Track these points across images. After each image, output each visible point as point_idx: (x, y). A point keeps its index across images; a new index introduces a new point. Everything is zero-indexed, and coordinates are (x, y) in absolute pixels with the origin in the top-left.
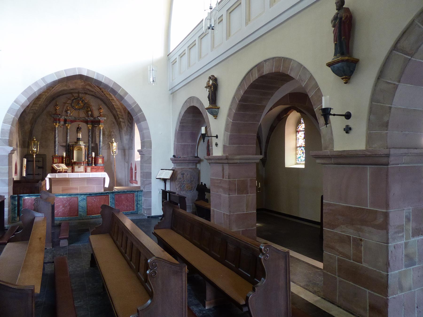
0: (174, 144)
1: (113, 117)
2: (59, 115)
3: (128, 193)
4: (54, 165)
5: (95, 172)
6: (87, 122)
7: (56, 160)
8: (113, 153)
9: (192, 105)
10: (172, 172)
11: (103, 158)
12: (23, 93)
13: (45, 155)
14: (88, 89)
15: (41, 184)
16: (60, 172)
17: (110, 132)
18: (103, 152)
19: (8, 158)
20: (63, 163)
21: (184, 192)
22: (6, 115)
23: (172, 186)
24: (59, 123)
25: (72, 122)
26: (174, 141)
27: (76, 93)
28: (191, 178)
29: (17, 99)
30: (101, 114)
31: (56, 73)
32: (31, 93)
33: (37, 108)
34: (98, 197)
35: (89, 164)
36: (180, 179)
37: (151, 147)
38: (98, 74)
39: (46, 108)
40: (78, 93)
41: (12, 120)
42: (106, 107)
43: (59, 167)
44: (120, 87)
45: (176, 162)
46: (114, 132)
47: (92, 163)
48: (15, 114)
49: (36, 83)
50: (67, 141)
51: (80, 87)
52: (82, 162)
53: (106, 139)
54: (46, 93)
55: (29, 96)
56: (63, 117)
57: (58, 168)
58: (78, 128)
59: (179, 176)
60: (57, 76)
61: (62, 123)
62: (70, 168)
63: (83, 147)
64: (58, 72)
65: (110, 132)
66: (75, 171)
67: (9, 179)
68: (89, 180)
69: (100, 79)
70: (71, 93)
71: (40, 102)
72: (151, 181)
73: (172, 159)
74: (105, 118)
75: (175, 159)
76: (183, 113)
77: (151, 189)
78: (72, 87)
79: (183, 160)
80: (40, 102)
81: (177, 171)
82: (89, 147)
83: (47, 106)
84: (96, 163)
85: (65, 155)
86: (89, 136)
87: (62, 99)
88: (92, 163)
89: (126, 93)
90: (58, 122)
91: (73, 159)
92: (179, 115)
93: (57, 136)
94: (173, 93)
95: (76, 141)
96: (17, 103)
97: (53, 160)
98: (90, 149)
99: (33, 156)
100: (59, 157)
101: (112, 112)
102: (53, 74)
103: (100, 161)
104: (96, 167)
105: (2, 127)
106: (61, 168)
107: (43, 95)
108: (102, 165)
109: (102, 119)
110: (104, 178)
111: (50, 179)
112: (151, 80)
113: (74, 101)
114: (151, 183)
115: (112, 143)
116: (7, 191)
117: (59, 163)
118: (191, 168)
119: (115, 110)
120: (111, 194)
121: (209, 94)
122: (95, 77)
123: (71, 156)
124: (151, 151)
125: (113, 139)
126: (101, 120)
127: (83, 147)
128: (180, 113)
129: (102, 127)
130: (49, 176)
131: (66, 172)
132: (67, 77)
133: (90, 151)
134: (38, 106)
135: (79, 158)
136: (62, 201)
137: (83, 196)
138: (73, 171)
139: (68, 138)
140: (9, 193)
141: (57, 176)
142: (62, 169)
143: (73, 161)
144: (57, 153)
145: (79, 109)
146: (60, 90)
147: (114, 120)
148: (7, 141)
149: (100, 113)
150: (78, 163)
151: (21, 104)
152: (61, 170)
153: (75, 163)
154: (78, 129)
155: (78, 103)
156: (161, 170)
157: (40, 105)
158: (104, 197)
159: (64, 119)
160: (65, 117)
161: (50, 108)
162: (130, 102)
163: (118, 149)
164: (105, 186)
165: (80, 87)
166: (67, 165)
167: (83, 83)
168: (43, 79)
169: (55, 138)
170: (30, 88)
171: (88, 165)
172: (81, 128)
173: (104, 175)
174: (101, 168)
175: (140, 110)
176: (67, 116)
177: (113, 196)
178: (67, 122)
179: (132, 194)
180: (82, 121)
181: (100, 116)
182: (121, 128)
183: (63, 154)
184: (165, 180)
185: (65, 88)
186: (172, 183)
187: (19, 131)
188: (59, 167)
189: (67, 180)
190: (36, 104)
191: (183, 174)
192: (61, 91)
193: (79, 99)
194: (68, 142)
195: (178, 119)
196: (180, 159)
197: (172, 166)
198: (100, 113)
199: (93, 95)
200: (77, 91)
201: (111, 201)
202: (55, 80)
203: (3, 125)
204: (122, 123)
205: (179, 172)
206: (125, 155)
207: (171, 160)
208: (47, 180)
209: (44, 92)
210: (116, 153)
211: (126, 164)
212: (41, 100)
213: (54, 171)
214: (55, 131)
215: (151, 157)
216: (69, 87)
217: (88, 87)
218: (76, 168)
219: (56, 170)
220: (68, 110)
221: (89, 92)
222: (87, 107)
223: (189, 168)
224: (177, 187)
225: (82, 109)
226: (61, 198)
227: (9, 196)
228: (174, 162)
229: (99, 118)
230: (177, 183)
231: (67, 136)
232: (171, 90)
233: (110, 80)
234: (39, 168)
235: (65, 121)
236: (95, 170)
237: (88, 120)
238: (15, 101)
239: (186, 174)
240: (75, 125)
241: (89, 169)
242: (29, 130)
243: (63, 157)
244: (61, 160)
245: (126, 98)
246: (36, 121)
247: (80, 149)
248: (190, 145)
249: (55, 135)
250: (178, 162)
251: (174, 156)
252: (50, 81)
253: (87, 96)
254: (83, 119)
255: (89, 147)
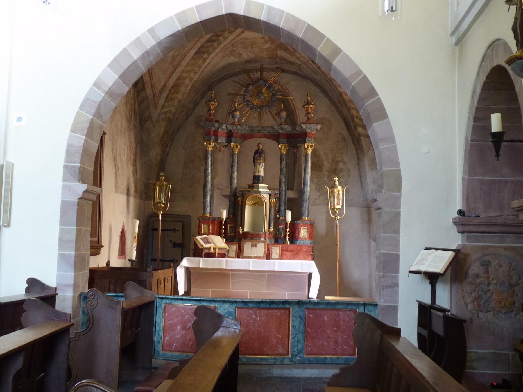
0: (463, 179)
1: (343, 124)
2: (217, 121)
3: (339, 307)
4: (198, 238)
5: (290, 259)
6: (276, 137)
7: (205, 228)
8: (334, 213)
9: (495, 64)
10: (449, 256)
11: (311, 226)
12: (110, 66)
13: (188, 217)
14: (284, 59)
15: (151, 276)
16: (210, 255)
17: (335, 162)
18: (312, 211)
19: (76, 207)
20: (220, 234)
21: (489, 315)
22: (78, 114)
23: (453, 298)
24: (216, 141)
25: (245, 137)
26: (464, 173)
27: (257, 70)
28: (511, 277)
29: (99, 78)
30: (310, 116)
31: (179, 16)
32: (126, 64)
33: (173, 109)
34: (263, 312)
35: (277, 239)
36: (477, 276)
37: (399, 188)
38: (270, 8)
39: (194, 109)
40: (261, 70)
41: (87, 125)
42: (325, 100)
43: (207, 242)
44: (321, 36)
45: (467, 228)
46: (344, 163)
47: (286, 236)
48: (93, 111)
49: (137, 42)
50: (231, 183)
51: (265, 54)
52: (262, 233)
53: (326, 179)
54: (192, 75)
55: (122, 71)
56: (224, 127)
57: (205, 246)
58: (257, 152)
59: (475, 269)
60: (180, 21)
61: (222, 140)
62: (234, 248)
63: (266, 197)
64: (183, 12)
65: (335, 162)
66: (245, 253)
67: (76, 256)
68: (273, 277)
69: (274, 21)
70: (247, 72)
71: (179, 96)
72: (397, 278)
73: (456, 223)
74: (319, 127)
75: (464, 221)
76: (479, 91)
77: (397, 301)
78: (246, 55)
79: (487, 225)
80: (179, 96)
81: (467, 256)
82: (279, 199)
83: (196, 104)
84: (293, 238)
85: (224, 216)
86: (281, 170)
87: (229, 86)
88: (284, 237)
89: (337, 51)
90: (213, 138)
91: (242, 226)
92: (473, 98)
93: (209, 171)
94: (460, 39)
95: (251, 182)
96: (99, 88)
97: (200, 226)
98: (283, 204)
99: (158, 216)
100: (213, 220)
101: (340, 112)
102: (172, 17)
103: (304, 232)
104: (293, 247)
105: (69, 140)
106: (211, 245)
107: (186, 78)
108: (308, 242)
109: (312, 128)
110: (310, 275)
111: (188, 271)
112: (387, 7)
113: (251, 87)
114: (396, 285)
115: (333, 186)
116: (71, 282)
117: (208, 234)
118: (511, 248)
119: (346, 105)
120: (296, 308)
121: (516, 18)
122: (263, 18)
123: (239, 217)
124: (400, 197)
125: (336, 179)
126: (308, 130)
127: (266, 197)
128: (474, 92)
129: (309, 148)
130: (185, 262)
131: (223, 256)
132: (202, 22)
133: (282, 208)
134: (176, 103)
135: (256, 223)
136: (182, 315)
137: (227, 306)
138: (240, 255)
139: (235, 175)
140: (75, 286)
141: (203, 263)
142: (215, 249)
143: (241, 229)
144: (208, 210)
145: (261, 107)
146: (222, 64)
147: (345, 133)
148: (77, 171)
149: (307, 113)
150: (253, 236)
151: (106, 89)
152: (212, 251)
153: (246, 236)
154: (258, 154)
155: (260, 93)
156: (426, 249)
157: (179, 101)
158: (278, 313)
159: (226, 131)
160: (230, 127)
161: (201, 111)
162: (347, 72)
163: (349, 204)
164: (310, 296)
165: (265, 54)
166: (229, 240)
167: (268, 45)
168: (151, 31)
169: (206, 176)
170: (125, 52)
171: (276, 242)
172: (263, 151)
173: (309, 266)
174: (304, 249)
175: (373, 92)
176: (233, 124)
177: (302, 314)
178: (233, 139)
179: (350, 310)
180: (266, 136)
181: (309, 121)
182: (362, 151)
183: (221, 214)
184: (432, 278)
185: (233, 59)
186: (454, 287)
187: (135, 161)
188: (208, 242)
189: (223, 275)
190: (172, 99)
191: (486, 265)
192: (224, 68)
193: (261, 82)
194: (235, 185)
195: (471, 107)
196: (477, 220)
197: (456, 240)
198: (307, 113)
199: (296, 74)
200: (257, 65)
201: (296, 323)
202: (178, 30)
203: (70, 136)
204: (362, 138)
205: (473, 257)
206: (369, 220)
207: (455, 223)
208: (181, 273)
209: (160, 62)
210: (340, 214)
211: (373, 243)
212: (182, 89)
213: (198, 252)
214: (206, 158)
215: (398, 215)
216: (241, 55)
217: (281, 53)
218: (247, 247)
219: (202, 249)
220: (236, 110)
221: (286, 67)
222: (281, 102)
223: (506, 248)
224: (469, 300)
225: (267, 106)
226: (179, 307)
227: (75, 291)
228: (461, 228)
229: (304, 126)
230: (467, 288)
231: (232, 172)
232: (456, 34)
233: (298, 21)
234: (175, 245)
235: (230, 136)
236: (289, 254)
237: (280, 131)
238: (96, 84)
239: (494, 263)
240: (252, 144)
241: (276, 250)
242: (159, 158)
243: (220, 221)
244: (216, 228)
245: (335, 63)
246: (172, 140)
247: (259, 203)
248: (507, 182)
249: (206, 170)
250: (472, 228)
251: (461, 212)
252: (164, 34)
253: (284, 75)
254: (269, 129)
255: (279, 199)
